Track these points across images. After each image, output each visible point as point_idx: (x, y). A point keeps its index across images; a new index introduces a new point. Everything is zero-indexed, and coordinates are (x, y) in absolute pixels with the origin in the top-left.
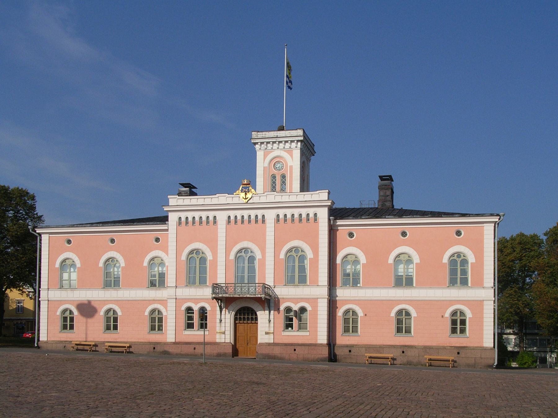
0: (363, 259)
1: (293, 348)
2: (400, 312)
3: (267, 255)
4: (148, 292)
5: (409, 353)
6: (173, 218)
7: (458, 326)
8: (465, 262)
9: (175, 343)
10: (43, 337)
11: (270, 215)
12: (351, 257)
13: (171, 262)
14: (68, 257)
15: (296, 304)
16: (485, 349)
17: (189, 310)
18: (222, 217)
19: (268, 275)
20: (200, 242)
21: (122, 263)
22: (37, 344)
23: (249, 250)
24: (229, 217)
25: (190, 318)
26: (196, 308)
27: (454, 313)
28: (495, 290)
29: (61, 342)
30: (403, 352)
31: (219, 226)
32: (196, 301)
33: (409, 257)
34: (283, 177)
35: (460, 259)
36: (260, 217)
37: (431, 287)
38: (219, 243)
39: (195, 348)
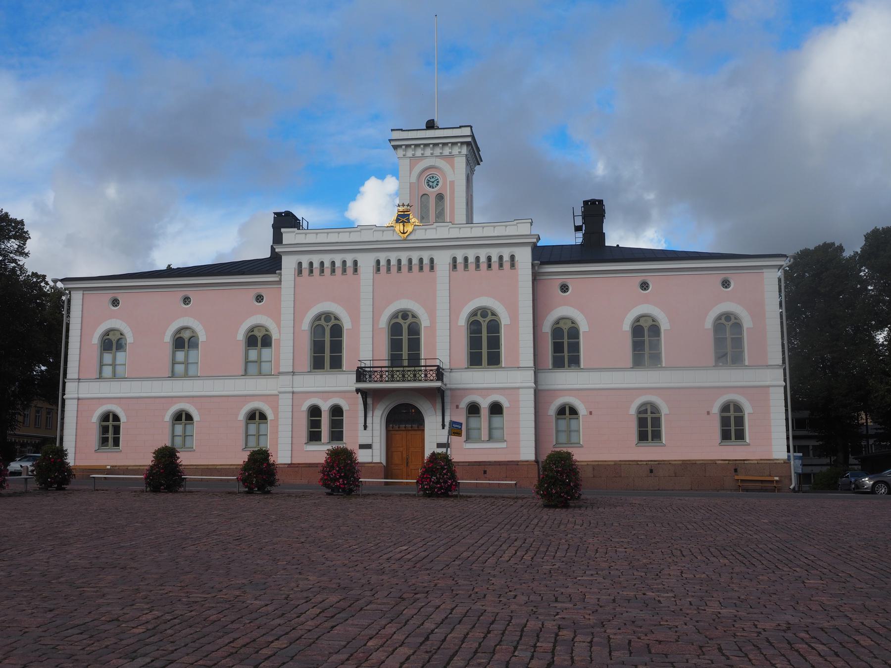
2: (106, 417)
7: (733, 428)
9: (290, 465)
12: (565, 324)
15: (325, 400)
16: (772, 464)
17: (315, 411)
24: (378, 262)
26: (325, 407)
27: (725, 408)
28: (785, 369)
31: (520, 272)
33: (653, 321)
34: (440, 197)
35: (730, 323)
36: (426, 261)
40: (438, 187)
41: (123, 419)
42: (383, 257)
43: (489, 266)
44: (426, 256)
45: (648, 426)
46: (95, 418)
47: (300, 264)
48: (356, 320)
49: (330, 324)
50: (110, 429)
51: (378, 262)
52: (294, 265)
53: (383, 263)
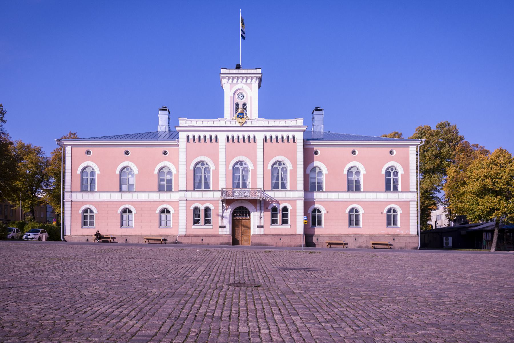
0: (363, 171)
1: (279, 238)
2: (86, 211)
3: (258, 166)
4: (158, 194)
5: (360, 240)
6: (183, 136)
7: (392, 220)
8: (396, 174)
9: (186, 235)
10: (68, 233)
11: (260, 137)
13: (180, 172)
14: (88, 165)
15: (202, 204)
16: (411, 236)
17: (196, 209)
18: (222, 137)
19: (258, 182)
20: (205, 155)
21: (136, 171)
22: (63, 238)
23: (244, 163)
24: (228, 137)
25: (206, 216)
29: (84, 236)
30: (356, 239)
31: (220, 144)
32: (202, 202)
37: (373, 192)
38: (220, 157)
39: (202, 240)
40: (244, 99)
41: (95, 212)
42: (230, 134)
43: (249, 141)
44: (252, 134)
45: (354, 218)
46: (192, 208)
47: (188, 137)
48: (217, 165)
49: (204, 167)
50: (87, 217)
51: (228, 137)
52: (185, 137)
53: (230, 137)
